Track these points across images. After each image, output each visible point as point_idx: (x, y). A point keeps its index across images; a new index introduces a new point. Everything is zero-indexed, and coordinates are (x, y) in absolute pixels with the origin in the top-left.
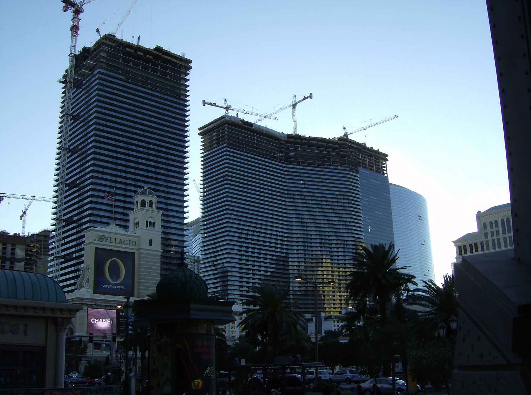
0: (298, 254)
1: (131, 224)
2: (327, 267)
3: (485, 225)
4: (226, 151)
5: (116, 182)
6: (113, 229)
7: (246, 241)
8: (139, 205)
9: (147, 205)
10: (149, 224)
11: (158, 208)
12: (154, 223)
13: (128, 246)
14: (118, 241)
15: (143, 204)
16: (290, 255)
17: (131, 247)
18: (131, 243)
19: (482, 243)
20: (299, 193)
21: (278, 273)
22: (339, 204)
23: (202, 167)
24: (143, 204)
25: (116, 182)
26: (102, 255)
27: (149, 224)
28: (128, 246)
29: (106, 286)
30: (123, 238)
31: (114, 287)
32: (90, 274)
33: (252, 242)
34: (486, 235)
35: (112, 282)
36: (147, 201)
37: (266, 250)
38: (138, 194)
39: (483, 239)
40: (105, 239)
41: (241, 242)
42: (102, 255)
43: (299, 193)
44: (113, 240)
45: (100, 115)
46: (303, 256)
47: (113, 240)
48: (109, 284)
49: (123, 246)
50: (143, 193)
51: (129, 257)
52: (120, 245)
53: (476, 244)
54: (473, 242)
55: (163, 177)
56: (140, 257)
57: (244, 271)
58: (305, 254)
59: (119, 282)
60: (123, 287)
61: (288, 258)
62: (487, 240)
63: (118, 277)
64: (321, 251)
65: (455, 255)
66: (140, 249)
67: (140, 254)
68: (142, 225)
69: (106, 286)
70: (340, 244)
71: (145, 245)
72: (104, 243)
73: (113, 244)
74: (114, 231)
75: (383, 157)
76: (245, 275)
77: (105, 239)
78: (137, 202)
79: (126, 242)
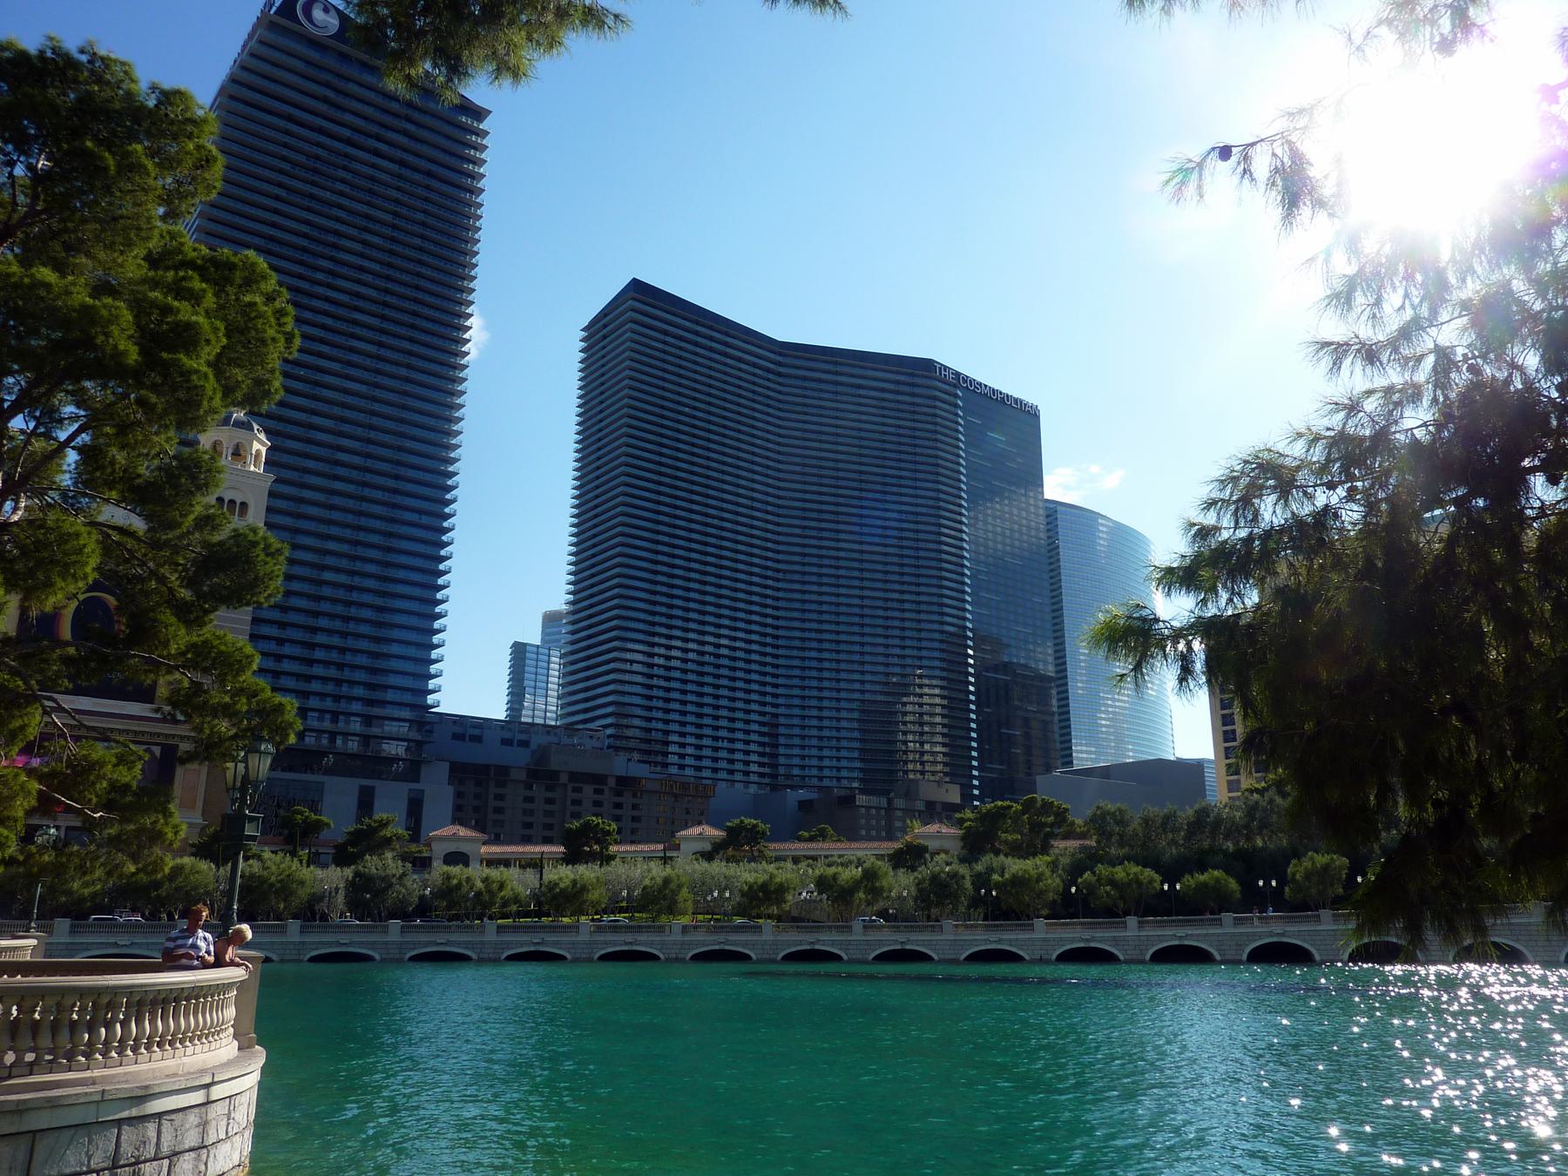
0: (803, 708)
2: (933, 734)
4: (623, 534)
5: (657, 542)
7: (701, 628)
16: (782, 720)
20: (815, 506)
22: (825, 571)
23: (573, 559)
25: (657, 542)
33: (716, 621)
37: (766, 606)
41: (654, 613)
43: (815, 506)
46: (815, 732)
55: (666, 539)
57: (706, 700)
58: (820, 709)
61: (777, 726)
64: (862, 644)
75: (638, 290)
76: (725, 692)
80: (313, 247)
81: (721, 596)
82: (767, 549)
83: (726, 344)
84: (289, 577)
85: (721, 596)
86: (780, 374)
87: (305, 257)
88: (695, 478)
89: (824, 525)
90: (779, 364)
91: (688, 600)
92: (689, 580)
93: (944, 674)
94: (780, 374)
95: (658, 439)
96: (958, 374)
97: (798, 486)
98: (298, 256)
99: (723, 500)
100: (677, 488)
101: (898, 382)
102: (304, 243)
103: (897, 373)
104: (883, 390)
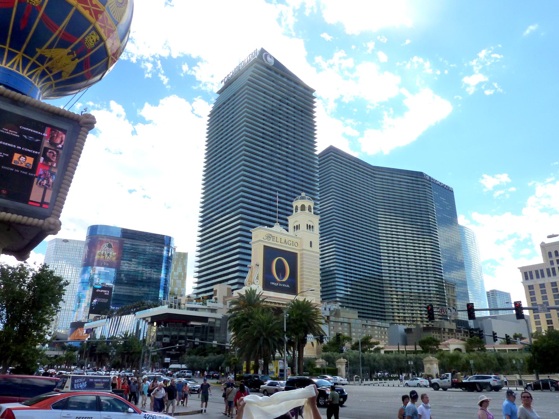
1: (291, 227)
3: (550, 254)
6: (277, 228)
8: (299, 209)
9: (307, 209)
10: (309, 227)
11: (315, 213)
12: (313, 226)
13: (291, 246)
14: (283, 241)
15: (303, 208)
17: (294, 247)
18: (293, 244)
19: (548, 270)
21: (353, 296)
24: (303, 208)
26: (270, 253)
27: (309, 227)
28: (291, 246)
29: (273, 283)
30: (288, 239)
31: (280, 285)
32: (259, 272)
34: (552, 263)
35: (278, 280)
36: (307, 206)
38: (297, 199)
39: (550, 267)
40: (272, 238)
42: (270, 253)
44: (279, 240)
45: (247, 153)
47: (279, 240)
48: (276, 281)
49: (287, 245)
50: (303, 198)
51: (292, 257)
52: (285, 245)
53: (531, 272)
54: (539, 269)
56: (301, 258)
59: (284, 280)
60: (288, 286)
62: (553, 267)
63: (284, 276)
65: (522, 280)
66: (303, 250)
67: (302, 254)
68: (303, 227)
69: (273, 283)
70: (424, 270)
71: (307, 246)
72: (271, 241)
73: (279, 243)
74: (279, 231)
77: (272, 238)
78: (297, 207)
79: (289, 242)
80: (275, 136)
81: (392, 231)
82: (346, 261)
83: (358, 167)
84: (542, 286)
85: (392, 231)
86: (374, 177)
87: (273, 140)
88: (350, 239)
89: (425, 237)
90: (374, 174)
91: (393, 247)
92: (419, 241)
93: (437, 289)
94: (374, 177)
95: (343, 220)
96: (430, 177)
97: (384, 225)
98: (271, 139)
99: (349, 230)
100: (350, 248)
101: (412, 180)
102: (273, 135)
103: (412, 177)
104: (408, 183)
